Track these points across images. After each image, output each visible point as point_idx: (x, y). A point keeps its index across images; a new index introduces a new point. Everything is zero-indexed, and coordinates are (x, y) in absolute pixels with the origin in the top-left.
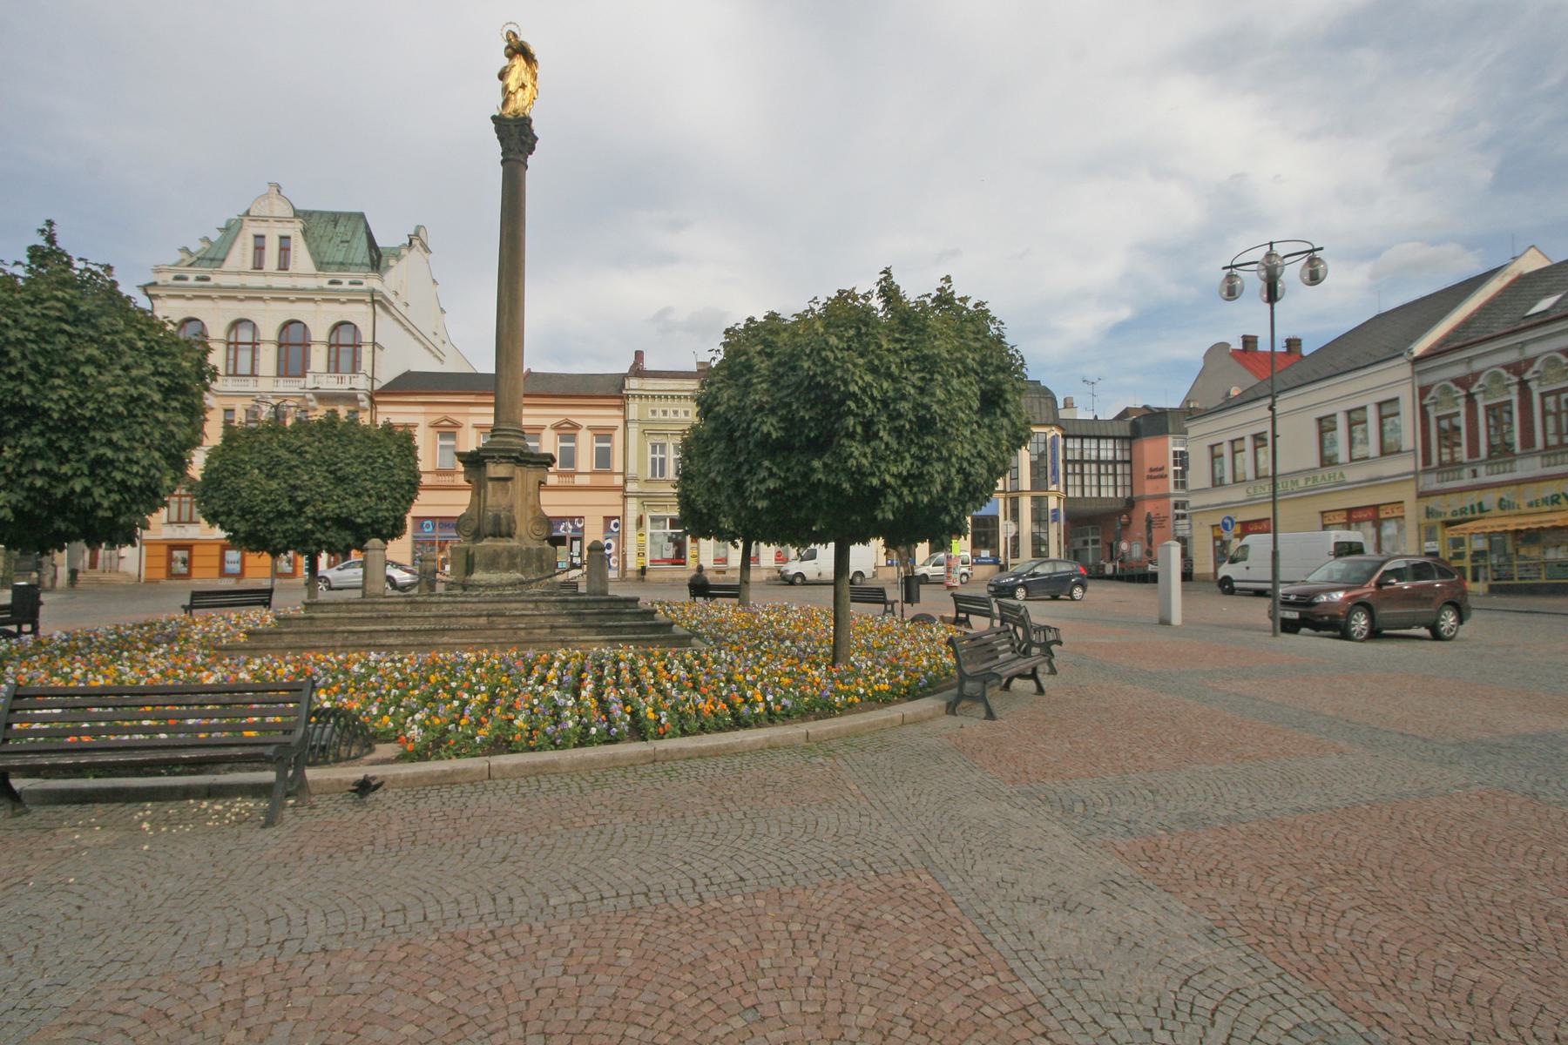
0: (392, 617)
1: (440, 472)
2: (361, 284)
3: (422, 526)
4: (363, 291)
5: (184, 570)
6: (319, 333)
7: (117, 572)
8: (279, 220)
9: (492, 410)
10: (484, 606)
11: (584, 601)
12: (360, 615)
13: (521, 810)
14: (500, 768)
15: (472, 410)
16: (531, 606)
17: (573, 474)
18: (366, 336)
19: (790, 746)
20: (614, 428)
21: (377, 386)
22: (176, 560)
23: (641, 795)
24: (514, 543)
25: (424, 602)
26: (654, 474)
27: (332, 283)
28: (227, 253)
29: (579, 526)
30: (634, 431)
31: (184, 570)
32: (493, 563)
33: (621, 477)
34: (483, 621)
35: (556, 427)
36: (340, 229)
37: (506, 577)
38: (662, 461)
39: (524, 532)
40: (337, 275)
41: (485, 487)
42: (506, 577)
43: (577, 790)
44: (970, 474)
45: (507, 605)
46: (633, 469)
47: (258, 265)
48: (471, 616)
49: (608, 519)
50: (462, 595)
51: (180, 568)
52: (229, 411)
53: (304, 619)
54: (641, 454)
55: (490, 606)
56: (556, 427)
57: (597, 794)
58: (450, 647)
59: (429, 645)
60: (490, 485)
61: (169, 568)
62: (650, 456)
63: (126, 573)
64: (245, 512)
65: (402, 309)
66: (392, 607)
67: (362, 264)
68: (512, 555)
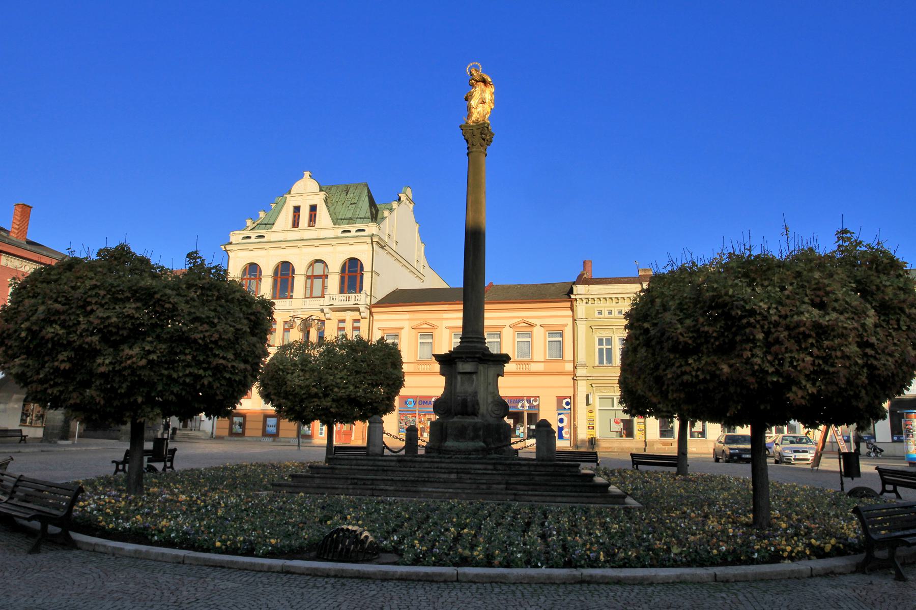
0: (387, 470)
1: (420, 362)
2: (364, 230)
3: (406, 403)
5: (240, 431)
6: (300, 269)
7: (199, 430)
8: (310, 194)
10: (454, 466)
11: (533, 465)
12: (365, 468)
13: (479, 602)
14: (465, 574)
15: (446, 315)
16: (490, 467)
18: (367, 267)
19: (701, 583)
20: (566, 325)
21: (374, 301)
22: (235, 424)
23: (568, 603)
24: (477, 420)
25: (411, 461)
26: (601, 361)
27: (344, 232)
28: (275, 220)
29: (535, 404)
30: (582, 327)
31: (240, 431)
32: (461, 434)
33: (572, 364)
34: (453, 476)
36: (350, 195)
37: (471, 445)
38: (609, 351)
39: (485, 412)
40: (347, 227)
41: (456, 378)
42: (471, 445)
43: (520, 596)
44: (876, 368)
45: (472, 466)
46: (581, 357)
47: (296, 224)
48: (445, 473)
49: (560, 399)
50: (438, 457)
51: (237, 429)
53: (328, 468)
54: (589, 346)
55: (459, 466)
57: (535, 599)
58: (428, 495)
59: (415, 492)
60: (459, 377)
61: (231, 429)
62: (597, 347)
63: (204, 431)
64: (286, 395)
65: (394, 246)
66: (388, 463)
67: (365, 218)
68: (476, 428)
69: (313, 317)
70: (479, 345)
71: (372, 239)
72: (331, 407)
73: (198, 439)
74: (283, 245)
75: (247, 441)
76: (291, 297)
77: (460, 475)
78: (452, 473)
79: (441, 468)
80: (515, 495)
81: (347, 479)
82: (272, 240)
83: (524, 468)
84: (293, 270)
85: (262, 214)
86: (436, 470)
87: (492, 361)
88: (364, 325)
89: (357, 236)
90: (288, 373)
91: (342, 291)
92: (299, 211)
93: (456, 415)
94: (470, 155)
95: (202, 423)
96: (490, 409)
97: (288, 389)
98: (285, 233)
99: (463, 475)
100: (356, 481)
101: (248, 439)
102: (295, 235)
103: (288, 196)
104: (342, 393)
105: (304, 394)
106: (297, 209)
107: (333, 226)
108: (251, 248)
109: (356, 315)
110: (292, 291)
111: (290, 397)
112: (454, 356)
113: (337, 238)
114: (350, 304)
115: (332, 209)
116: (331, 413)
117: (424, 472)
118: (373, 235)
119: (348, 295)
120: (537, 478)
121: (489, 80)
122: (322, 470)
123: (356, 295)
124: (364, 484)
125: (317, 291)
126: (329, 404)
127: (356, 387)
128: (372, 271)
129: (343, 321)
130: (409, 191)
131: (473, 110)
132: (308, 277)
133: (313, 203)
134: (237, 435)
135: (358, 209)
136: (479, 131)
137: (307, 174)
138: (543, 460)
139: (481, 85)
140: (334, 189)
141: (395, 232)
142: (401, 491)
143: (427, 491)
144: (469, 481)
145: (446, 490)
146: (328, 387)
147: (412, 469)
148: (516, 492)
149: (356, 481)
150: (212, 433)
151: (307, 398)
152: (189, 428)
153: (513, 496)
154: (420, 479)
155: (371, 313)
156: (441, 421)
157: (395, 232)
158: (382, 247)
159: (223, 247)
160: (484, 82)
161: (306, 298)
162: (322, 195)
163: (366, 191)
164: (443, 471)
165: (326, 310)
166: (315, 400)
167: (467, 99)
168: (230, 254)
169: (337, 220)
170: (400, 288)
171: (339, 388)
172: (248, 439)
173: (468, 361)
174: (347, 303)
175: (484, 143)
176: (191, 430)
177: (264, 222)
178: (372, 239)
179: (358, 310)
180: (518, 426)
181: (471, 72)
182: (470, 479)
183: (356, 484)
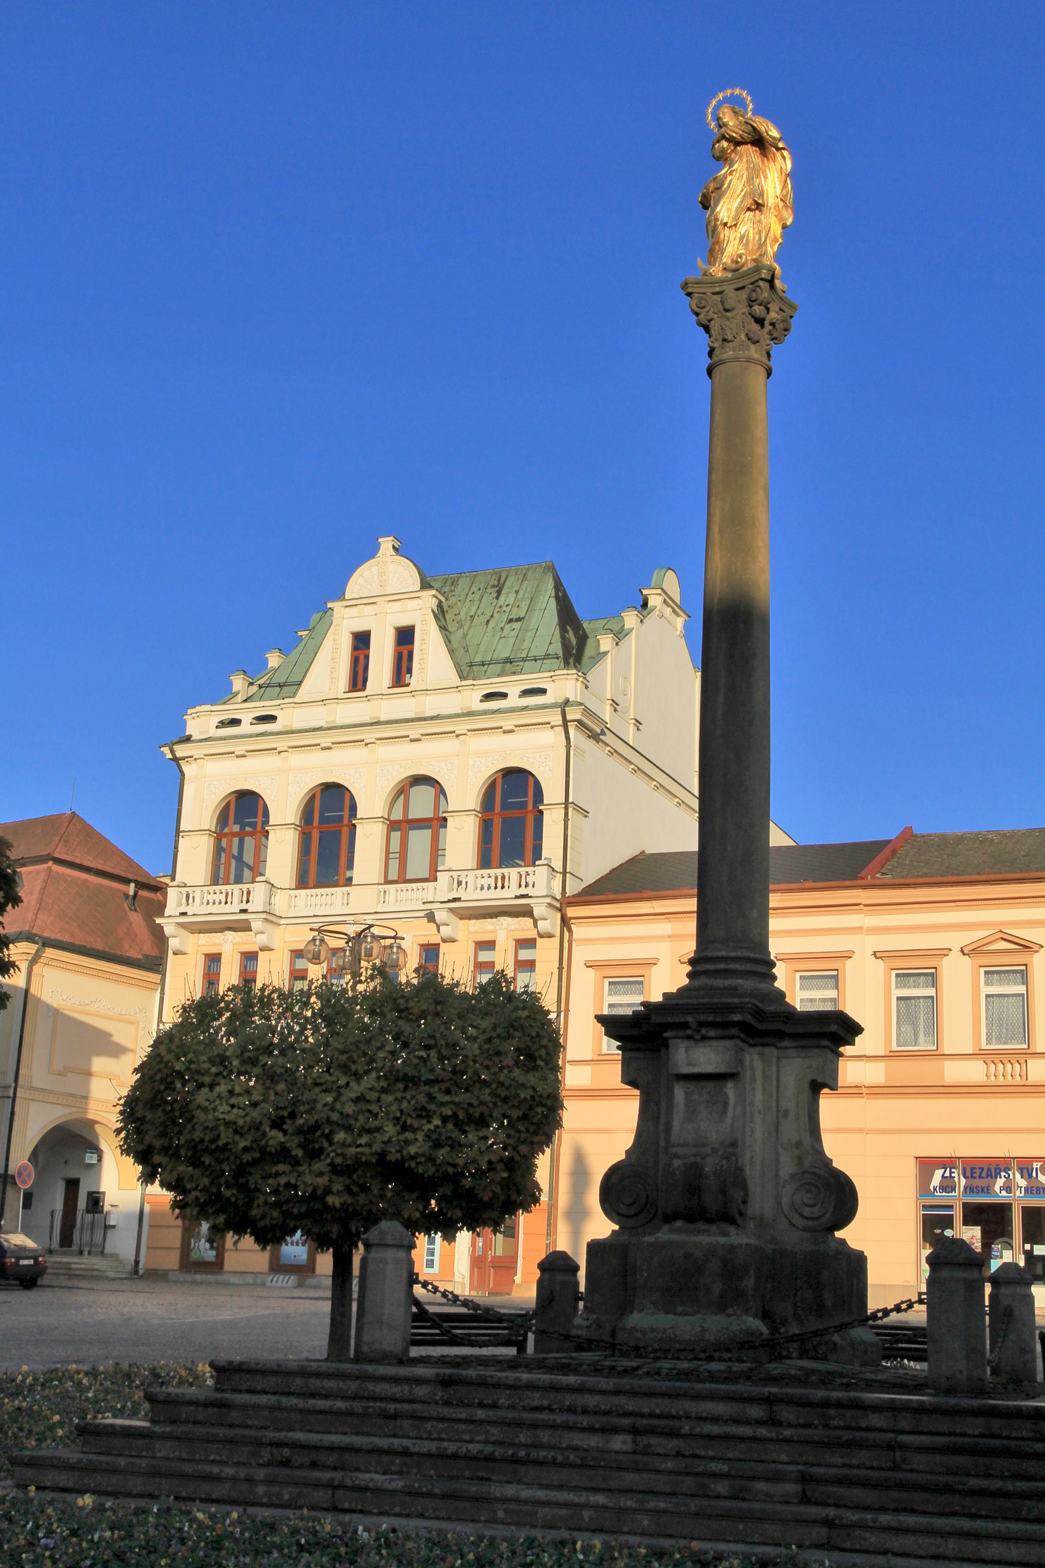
2: (543, 691)
4: (545, 707)
5: (211, 1255)
7: (102, 1253)
8: (396, 597)
9: (694, 901)
16: (756, 1412)
17: (939, 1055)
18: (552, 792)
27: (489, 697)
31: (211, 1255)
34: (620, 1443)
35: (970, 951)
36: (507, 597)
41: (670, 1092)
47: (358, 680)
48: (590, 1430)
52: (213, 960)
56: (970, 951)
59: (476, 1499)
60: (679, 1092)
63: (115, 1256)
65: (630, 734)
67: (547, 656)
69: (376, 931)
70: (763, 986)
71: (564, 714)
72: (328, 1191)
73: (97, 1278)
74: (325, 740)
75: (228, 1284)
76: (349, 882)
77: (644, 1440)
78: (615, 1430)
79: (585, 1412)
80: (829, 1523)
81: (259, 1443)
82: (296, 726)
83: (875, 1420)
84: (353, 808)
85: (274, 660)
86: (559, 1418)
87: (794, 1036)
88: (546, 954)
89: (524, 709)
90: (200, 1086)
91: (484, 861)
92: (368, 646)
93: (668, 1219)
94: (716, 372)
95: (110, 1232)
96: (785, 1201)
97: (197, 1135)
98: (331, 707)
99: (653, 1440)
100: (286, 1452)
101: (234, 1280)
102: (357, 710)
103: (336, 606)
104: (365, 1148)
105: (246, 1149)
106: (362, 640)
107: (457, 681)
108: (240, 749)
109: (522, 927)
110: (350, 865)
111: (207, 1160)
112: (656, 1019)
113: (470, 714)
114: (506, 896)
115: (457, 637)
116: (327, 1208)
117: (519, 1424)
118: (567, 702)
119: (499, 872)
120: (919, 1461)
121: (775, 133)
122: (187, 1411)
123: (523, 870)
124: (314, 1465)
125: (418, 864)
126: (322, 1181)
127: (405, 1128)
128: (567, 802)
129: (489, 945)
130: (671, 582)
131: (725, 234)
132: (393, 826)
133: (404, 622)
134: (202, 1266)
135: (530, 635)
136: (744, 295)
137: (387, 544)
138: (950, 1391)
139: (750, 152)
140: (464, 583)
141: (631, 695)
142: (430, 1495)
143: (518, 1500)
144: (669, 1465)
145: (582, 1498)
146: (317, 1126)
147: (481, 1414)
148: (831, 1512)
149: (286, 1452)
150: (137, 1262)
151: (255, 1162)
152: (75, 1248)
153: (824, 1531)
154: (499, 1452)
155: (565, 922)
156: (624, 1238)
157: (631, 695)
158: (595, 737)
159: (166, 750)
160: (759, 142)
161: (387, 882)
162: (429, 600)
163: (550, 585)
164: (585, 1421)
165: (441, 916)
166: (281, 1167)
167: (706, 204)
168: (186, 768)
169: (471, 665)
170: (649, 851)
171: (349, 1129)
172: (234, 1280)
173: (704, 1038)
174: (499, 893)
175: (764, 334)
176: (81, 1253)
177: (275, 680)
178: (564, 714)
179: (527, 912)
180: (996, 1247)
181: (718, 119)
182: (679, 1454)
183: (286, 1463)
